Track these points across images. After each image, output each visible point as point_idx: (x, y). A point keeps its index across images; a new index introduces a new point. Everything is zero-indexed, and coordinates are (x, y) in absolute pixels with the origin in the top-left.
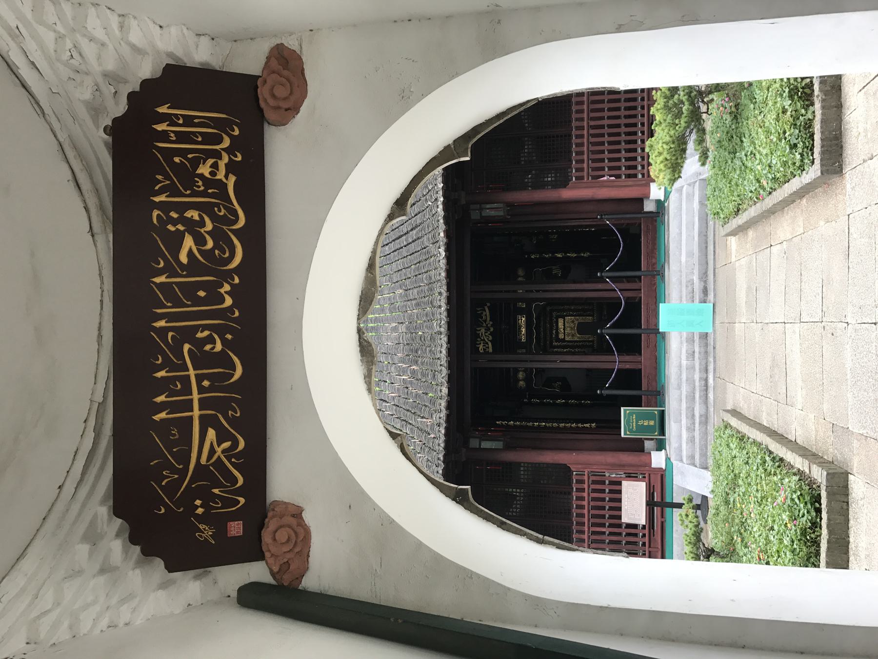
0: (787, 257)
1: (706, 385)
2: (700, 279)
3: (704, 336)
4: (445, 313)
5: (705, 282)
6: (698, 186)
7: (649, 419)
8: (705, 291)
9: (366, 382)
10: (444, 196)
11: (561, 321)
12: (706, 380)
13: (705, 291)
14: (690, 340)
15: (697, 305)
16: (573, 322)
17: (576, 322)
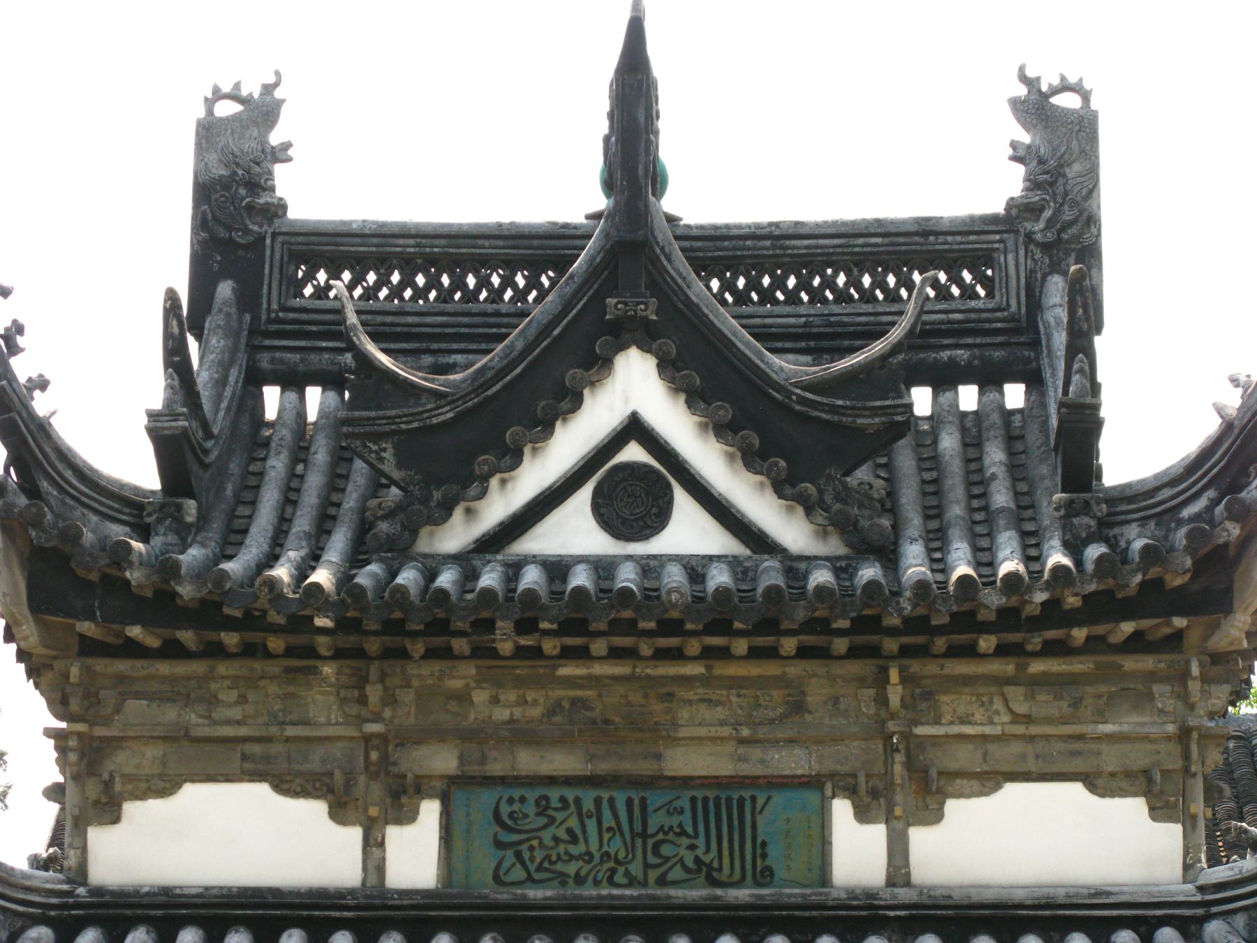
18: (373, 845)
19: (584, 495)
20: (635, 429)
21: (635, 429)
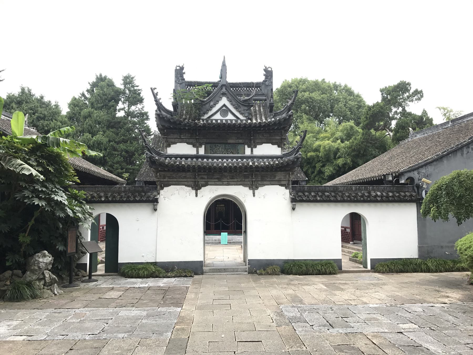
0: (131, 334)
1: (209, 243)
2: (233, 242)
3: (220, 243)
4: (455, 117)
5: (232, 243)
6: (334, 180)
7: (396, 131)
8: (230, 243)
9: (336, 87)
10: (91, 230)
11: (223, 205)
12: (210, 243)
13: (230, 243)
14: (219, 240)
15: (227, 241)
16: (223, 210)
17: (223, 211)
18: (252, 151)
19: (219, 113)
20: (224, 105)
21: (224, 105)
